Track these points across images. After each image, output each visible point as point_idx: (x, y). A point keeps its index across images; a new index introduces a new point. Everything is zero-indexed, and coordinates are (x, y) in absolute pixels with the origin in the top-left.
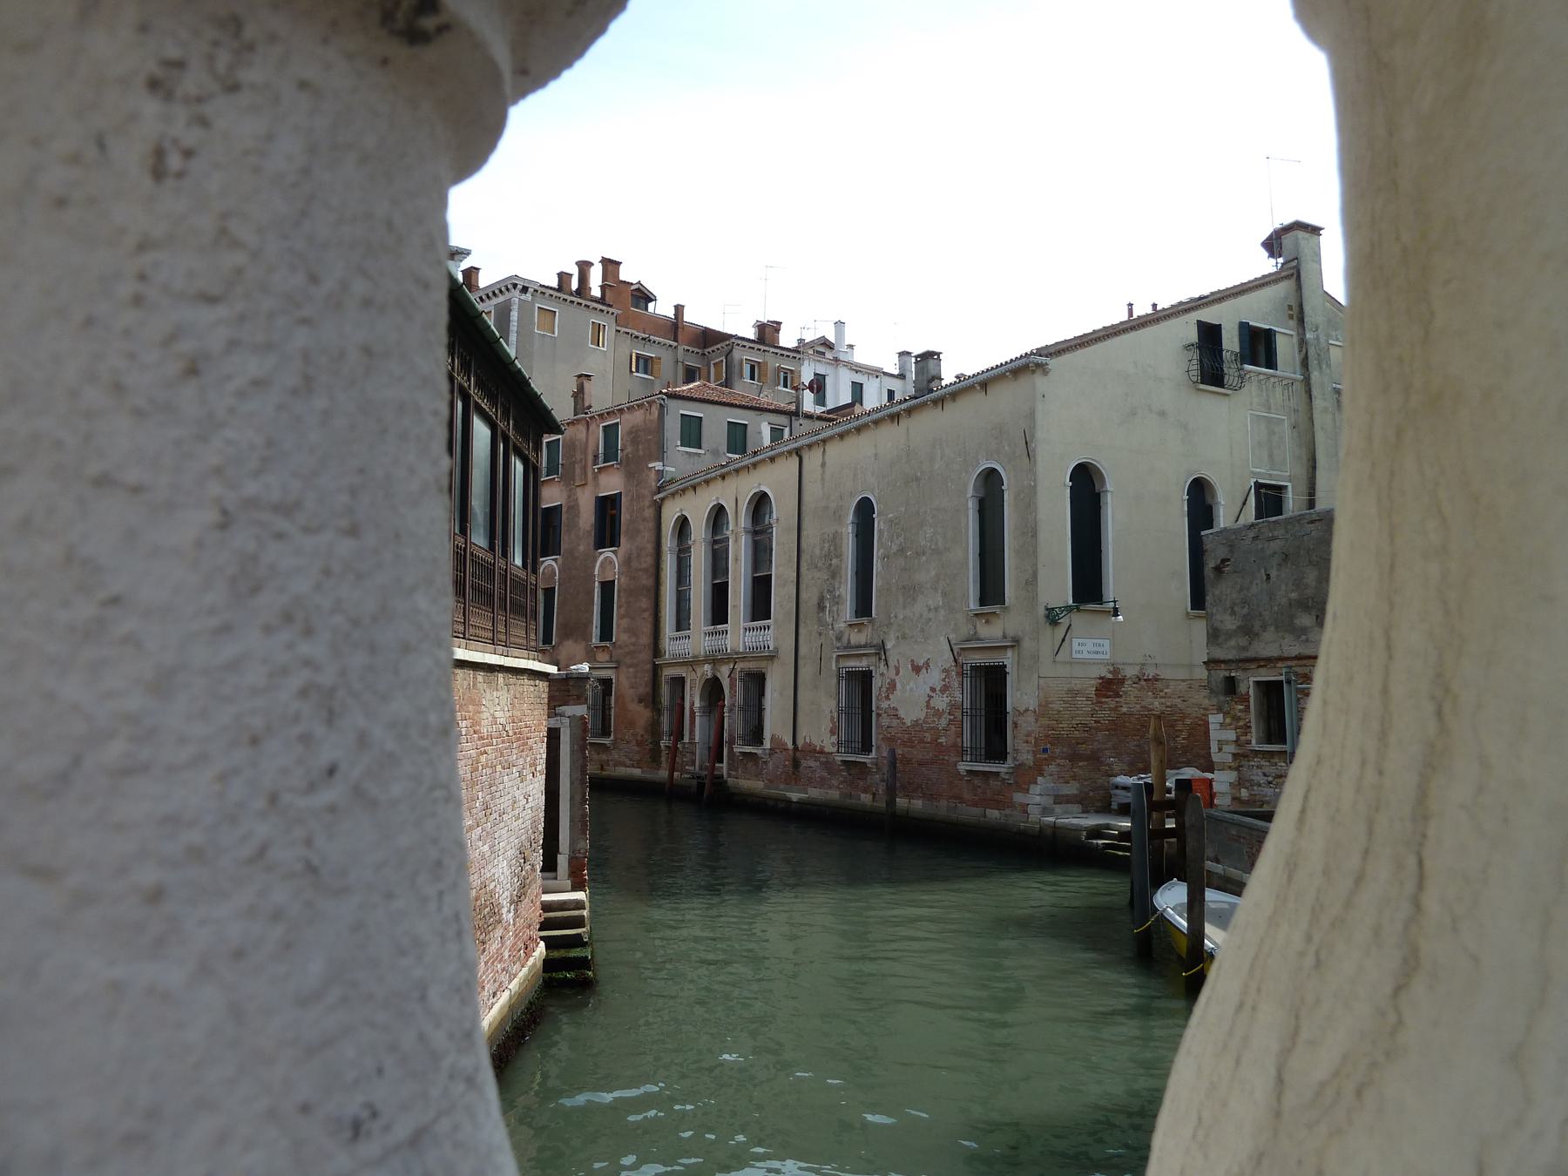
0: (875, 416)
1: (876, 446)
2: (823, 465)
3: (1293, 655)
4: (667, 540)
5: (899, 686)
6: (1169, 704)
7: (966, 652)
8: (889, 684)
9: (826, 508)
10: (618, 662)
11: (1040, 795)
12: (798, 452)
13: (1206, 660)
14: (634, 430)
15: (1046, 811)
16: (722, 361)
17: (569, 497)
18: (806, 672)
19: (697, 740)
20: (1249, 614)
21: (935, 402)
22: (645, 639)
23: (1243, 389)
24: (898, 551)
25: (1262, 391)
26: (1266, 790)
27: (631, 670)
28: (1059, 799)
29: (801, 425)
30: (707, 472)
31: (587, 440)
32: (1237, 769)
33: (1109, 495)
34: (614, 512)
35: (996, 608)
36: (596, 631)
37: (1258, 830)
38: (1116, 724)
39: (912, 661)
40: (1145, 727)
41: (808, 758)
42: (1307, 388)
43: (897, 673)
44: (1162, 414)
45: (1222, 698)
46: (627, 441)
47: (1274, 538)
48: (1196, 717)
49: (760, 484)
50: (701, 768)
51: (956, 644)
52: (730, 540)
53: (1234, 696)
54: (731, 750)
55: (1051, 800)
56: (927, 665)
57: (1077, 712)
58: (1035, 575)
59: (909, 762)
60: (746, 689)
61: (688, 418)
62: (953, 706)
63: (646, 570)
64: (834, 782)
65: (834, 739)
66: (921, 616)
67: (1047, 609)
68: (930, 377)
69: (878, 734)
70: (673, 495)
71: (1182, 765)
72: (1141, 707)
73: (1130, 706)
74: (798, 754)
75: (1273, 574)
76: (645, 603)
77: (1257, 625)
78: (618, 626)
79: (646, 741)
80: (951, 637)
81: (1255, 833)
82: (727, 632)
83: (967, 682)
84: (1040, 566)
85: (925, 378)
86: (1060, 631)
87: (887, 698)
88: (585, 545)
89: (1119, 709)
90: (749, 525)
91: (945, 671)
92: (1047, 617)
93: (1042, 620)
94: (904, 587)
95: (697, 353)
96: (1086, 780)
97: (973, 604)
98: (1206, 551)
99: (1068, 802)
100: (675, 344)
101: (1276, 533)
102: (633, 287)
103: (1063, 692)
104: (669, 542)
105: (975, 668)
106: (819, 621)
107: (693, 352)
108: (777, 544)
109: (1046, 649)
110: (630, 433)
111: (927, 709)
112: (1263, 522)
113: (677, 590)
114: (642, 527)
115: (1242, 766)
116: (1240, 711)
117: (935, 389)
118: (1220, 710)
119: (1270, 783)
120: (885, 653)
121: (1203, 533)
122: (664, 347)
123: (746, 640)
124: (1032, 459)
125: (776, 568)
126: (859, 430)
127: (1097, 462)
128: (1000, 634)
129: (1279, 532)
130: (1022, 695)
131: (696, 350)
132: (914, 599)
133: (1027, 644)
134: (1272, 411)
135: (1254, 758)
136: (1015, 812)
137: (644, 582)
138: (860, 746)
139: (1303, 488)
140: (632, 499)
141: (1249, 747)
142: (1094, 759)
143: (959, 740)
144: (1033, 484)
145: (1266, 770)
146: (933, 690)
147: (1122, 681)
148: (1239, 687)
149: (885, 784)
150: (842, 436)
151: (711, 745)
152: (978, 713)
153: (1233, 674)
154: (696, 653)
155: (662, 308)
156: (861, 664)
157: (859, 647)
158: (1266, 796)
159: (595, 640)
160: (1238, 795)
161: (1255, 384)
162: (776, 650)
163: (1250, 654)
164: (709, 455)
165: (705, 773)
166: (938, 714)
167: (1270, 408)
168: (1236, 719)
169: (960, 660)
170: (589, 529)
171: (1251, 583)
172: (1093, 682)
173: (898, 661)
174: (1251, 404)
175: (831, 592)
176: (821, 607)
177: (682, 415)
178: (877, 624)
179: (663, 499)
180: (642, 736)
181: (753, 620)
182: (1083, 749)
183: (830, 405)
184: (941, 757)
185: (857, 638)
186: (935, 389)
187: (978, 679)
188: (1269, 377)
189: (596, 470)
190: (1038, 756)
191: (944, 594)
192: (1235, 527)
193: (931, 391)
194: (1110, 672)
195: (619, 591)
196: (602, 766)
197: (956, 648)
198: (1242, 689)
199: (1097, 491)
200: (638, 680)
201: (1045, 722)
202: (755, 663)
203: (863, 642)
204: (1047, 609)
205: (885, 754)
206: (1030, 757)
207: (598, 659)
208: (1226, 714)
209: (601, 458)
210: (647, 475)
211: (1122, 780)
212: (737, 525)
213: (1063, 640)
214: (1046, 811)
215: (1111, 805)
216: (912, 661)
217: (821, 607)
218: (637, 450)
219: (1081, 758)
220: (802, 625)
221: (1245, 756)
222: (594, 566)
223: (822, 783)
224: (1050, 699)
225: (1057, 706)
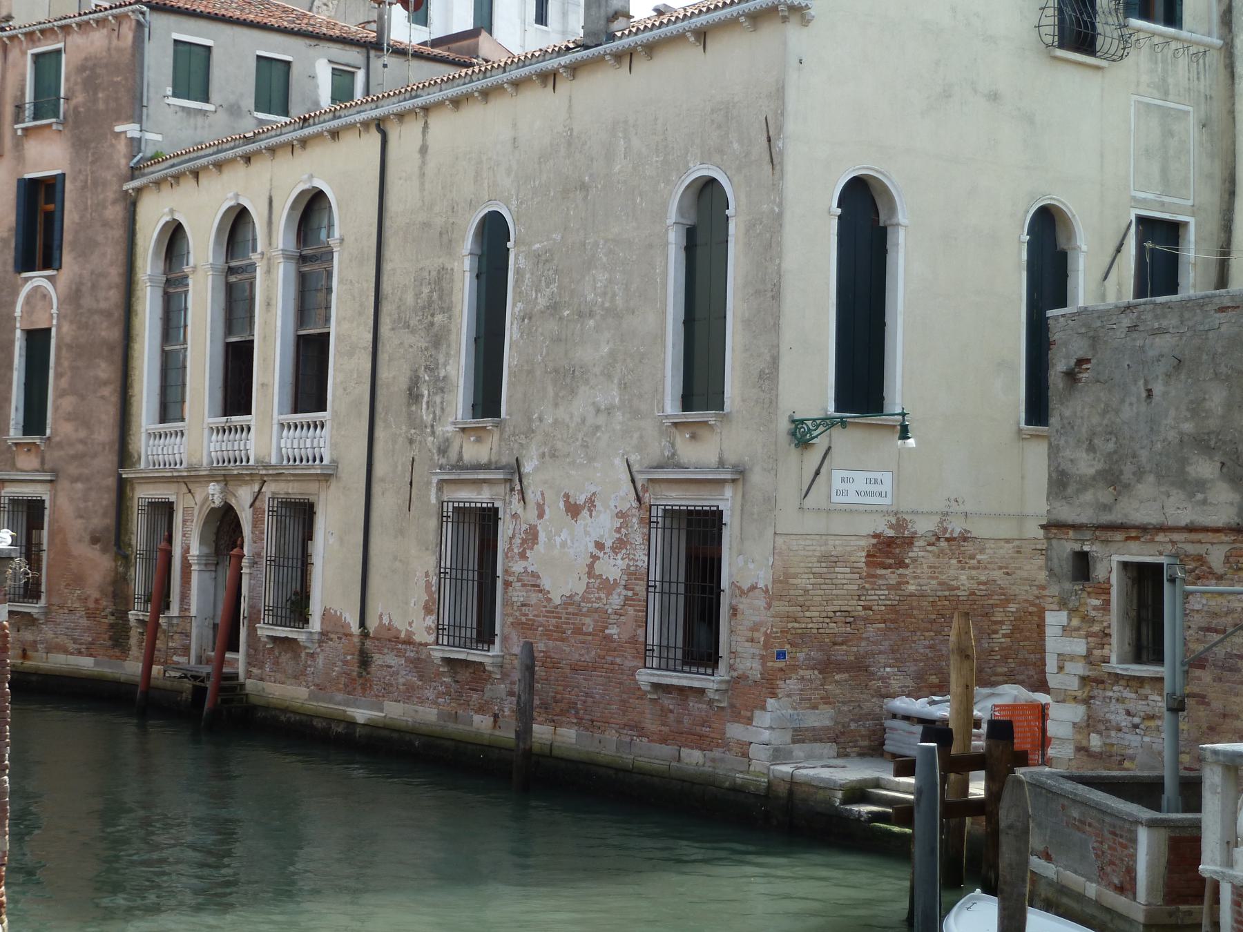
0: (516, 74)
1: (515, 125)
2: (424, 150)
3: (1183, 524)
4: (145, 260)
5: (542, 536)
6: (983, 578)
7: (657, 488)
8: (526, 532)
9: (426, 225)
10: (53, 471)
11: (771, 728)
12: (380, 125)
13: (1044, 522)
14: (90, 64)
15: (779, 755)
18: (385, 504)
19: (193, 612)
20: (1115, 452)
21: (618, 57)
22: (105, 433)
23: (1125, 60)
24: (548, 308)
25: (1156, 63)
26: (1128, 736)
27: (79, 486)
28: (801, 736)
29: (385, 66)
30: (220, 147)
32: (1087, 701)
33: (902, 233)
34: (51, 207)
35: (709, 416)
37: (1111, 815)
38: (897, 612)
39: (567, 496)
40: (943, 616)
41: (386, 651)
42: (1228, 61)
43: (541, 515)
44: (994, 97)
45: (1067, 585)
46: (76, 83)
47: (1161, 332)
48: (1026, 601)
49: (311, 176)
50: (200, 660)
51: (640, 472)
52: (258, 269)
53: (1087, 584)
54: (252, 631)
55: (788, 737)
56: (591, 503)
57: (834, 592)
58: (775, 361)
59: (555, 665)
60: (281, 528)
61: (187, 48)
62: (630, 573)
63: (107, 314)
64: (430, 694)
65: (431, 621)
66: (583, 421)
67: (793, 421)
68: (611, 11)
69: (504, 615)
70: (158, 183)
71: (1001, 678)
72: (940, 584)
73: (922, 582)
74: (368, 643)
75: (1158, 389)
76: (105, 370)
77: (1128, 470)
78: (56, 409)
79: (104, 610)
80: (633, 458)
81: (1107, 819)
82: (249, 429)
83: (657, 537)
84: (784, 348)
85: (603, 12)
86: (814, 457)
87: (523, 556)
89: (903, 587)
90: (292, 246)
91: (621, 515)
92: (793, 434)
93: (783, 438)
94: (556, 371)
96: (844, 703)
97: (671, 406)
98: (1054, 343)
99: (815, 740)
101: (1165, 323)
103: (815, 560)
104: (148, 265)
105: (670, 513)
106: (410, 418)
108: (340, 281)
109: (788, 492)
110: (82, 68)
111: (589, 578)
112: (1145, 304)
113: (163, 351)
114: (100, 238)
115: (1092, 697)
116: (1095, 608)
117: (619, 34)
118: (1063, 604)
119: (1136, 726)
120: (520, 481)
121: (1050, 313)
123: (283, 445)
124: (778, 167)
125: (338, 323)
126: (486, 94)
127: (884, 175)
128: (713, 459)
129: (1171, 321)
130: (746, 562)
132: (573, 392)
133: (757, 477)
134: (1171, 97)
135: (1113, 685)
136: (728, 756)
137: (103, 334)
138: (474, 635)
139: (1213, 224)
140: (84, 187)
141: (1106, 668)
142: (860, 668)
143: (641, 632)
144: (777, 210)
145: (1131, 706)
146: (599, 546)
147: (909, 542)
148: (1095, 568)
149: (514, 699)
150: (456, 102)
151: (218, 621)
152: (674, 590)
153: (1086, 548)
154: (194, 461)
156: (480, 497)
157: (478, 467)
158: (1128, 747)
159: (14, 432)
160: (1084, 743)
161: (1145, 50)
162: (335, 463)
163: (1114, 517)
164: (222, 117)
165: (206, 669)
166: (607, 586)
167: (1166, 93)
168: (1086, 619)
169: (646, 497)
170: (5, 235)
171: (1123, 401)
172: (863, 543)
173: (542, 494)
174: (1138, 84)
175: (431, 370)
176: (413, 396)
177: (176, 41)
178: (508, 430)
179: (139, 190)
180: (97, 601)
181: (296, 410)
182: (840, 653)
183: (437, 29)
184: (609, 659)
185: (474, 451)
186: (619, 34)
187: (675, 532)
188: (1169, 40)
189: (19, 132)
190: (770, 664)
191: (624, 386)
192: (1101, 308)
193: (612, 37)
194: (891, 527)
195: (58, 348)
196: (24, 651)
197: (640, 479)
198: (1099, 572)
199: (881, 224)
200: (90, 504)
201: (780, 607)
202: (296, 485)
203: (484, 459)
204: (793, 421)
205: (516, 650)
206: (757, 665)
207: (19, 465)
208: (1073, 611)
209: (29, 111)
210: (112, 146)
211: (903, 704)
212: (270, 244)
213: (817, 473)
214: (779, 755)
215: (883, 744)
216: (567, 496)
217: (413, 396)
218: (95, 100)
219: (840, 667)
221: (1099, 681)
222: (14, 303)
223: (409, 694)
224: (792, 571)
225: (803, 582)
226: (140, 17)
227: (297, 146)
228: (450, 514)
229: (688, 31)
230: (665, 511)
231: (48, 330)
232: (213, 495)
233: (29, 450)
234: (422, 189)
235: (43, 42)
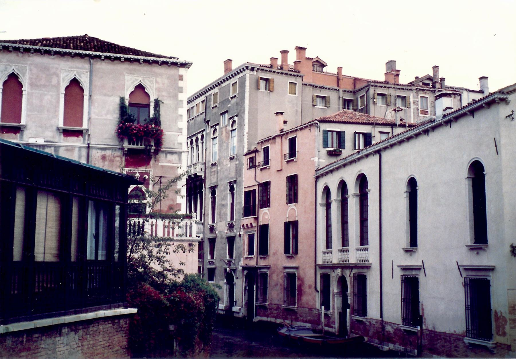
16: (364, 95)
98: (491, 285)
102: (314, 60)
104: (320, 200)
155: (331, 69)
227: (357, 160)
228: (468, 283)
229: (483, 104)
230: (470, 280)
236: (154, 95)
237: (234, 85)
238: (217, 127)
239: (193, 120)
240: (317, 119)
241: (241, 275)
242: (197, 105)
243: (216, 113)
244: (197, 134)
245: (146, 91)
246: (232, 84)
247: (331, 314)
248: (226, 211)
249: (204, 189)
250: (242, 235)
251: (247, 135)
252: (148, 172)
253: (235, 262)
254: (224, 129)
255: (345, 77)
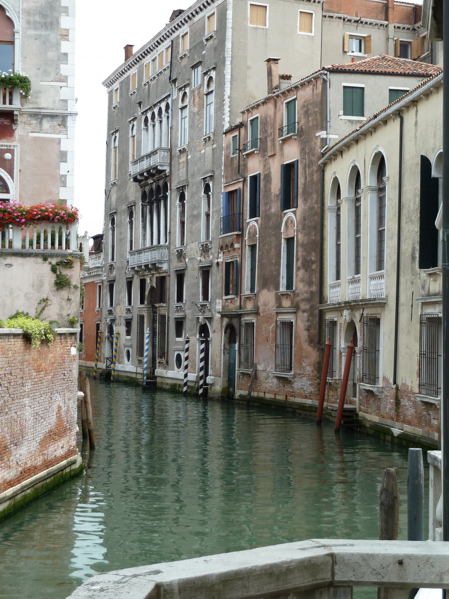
4: (247, 207)
14: (306, 103)
17: (265, 166)
31: (275, 116)
36: (283, 281)
46: (301, 115)
61: (351, 89)
88: (275, 207)
95: (408, 29)
100: (386, 23)
107: (404, 28)
122: (376, 27)
131: (407, 26)
159: (283, 289)
170: (68, 205)
177: (345, 87)
189: (280, 142)
209: (285, 129)
220: (401, 274)
226: (325, 77)
231: (293, 238)
232: (345, 316)
233: (287, 298)
234: (416, 145)
235: (289, 96)
236: (21, 20)
237: (211, 18)
238: (187, 90)
239: (155, 80)
240: (326, 67)
241: (219, 326)
242: (159, 54)
243: (185, 66)
244: (160, 102)
245: (7, 14)
246: (209, 17)
247: (379, 392)
248: (200, 226)
249: (169, 191)
250: (220, 263)
251: (229, 100)
252: (12, 148)
253: (210, 307)
254: (196, 92)
255: (399, 4)
